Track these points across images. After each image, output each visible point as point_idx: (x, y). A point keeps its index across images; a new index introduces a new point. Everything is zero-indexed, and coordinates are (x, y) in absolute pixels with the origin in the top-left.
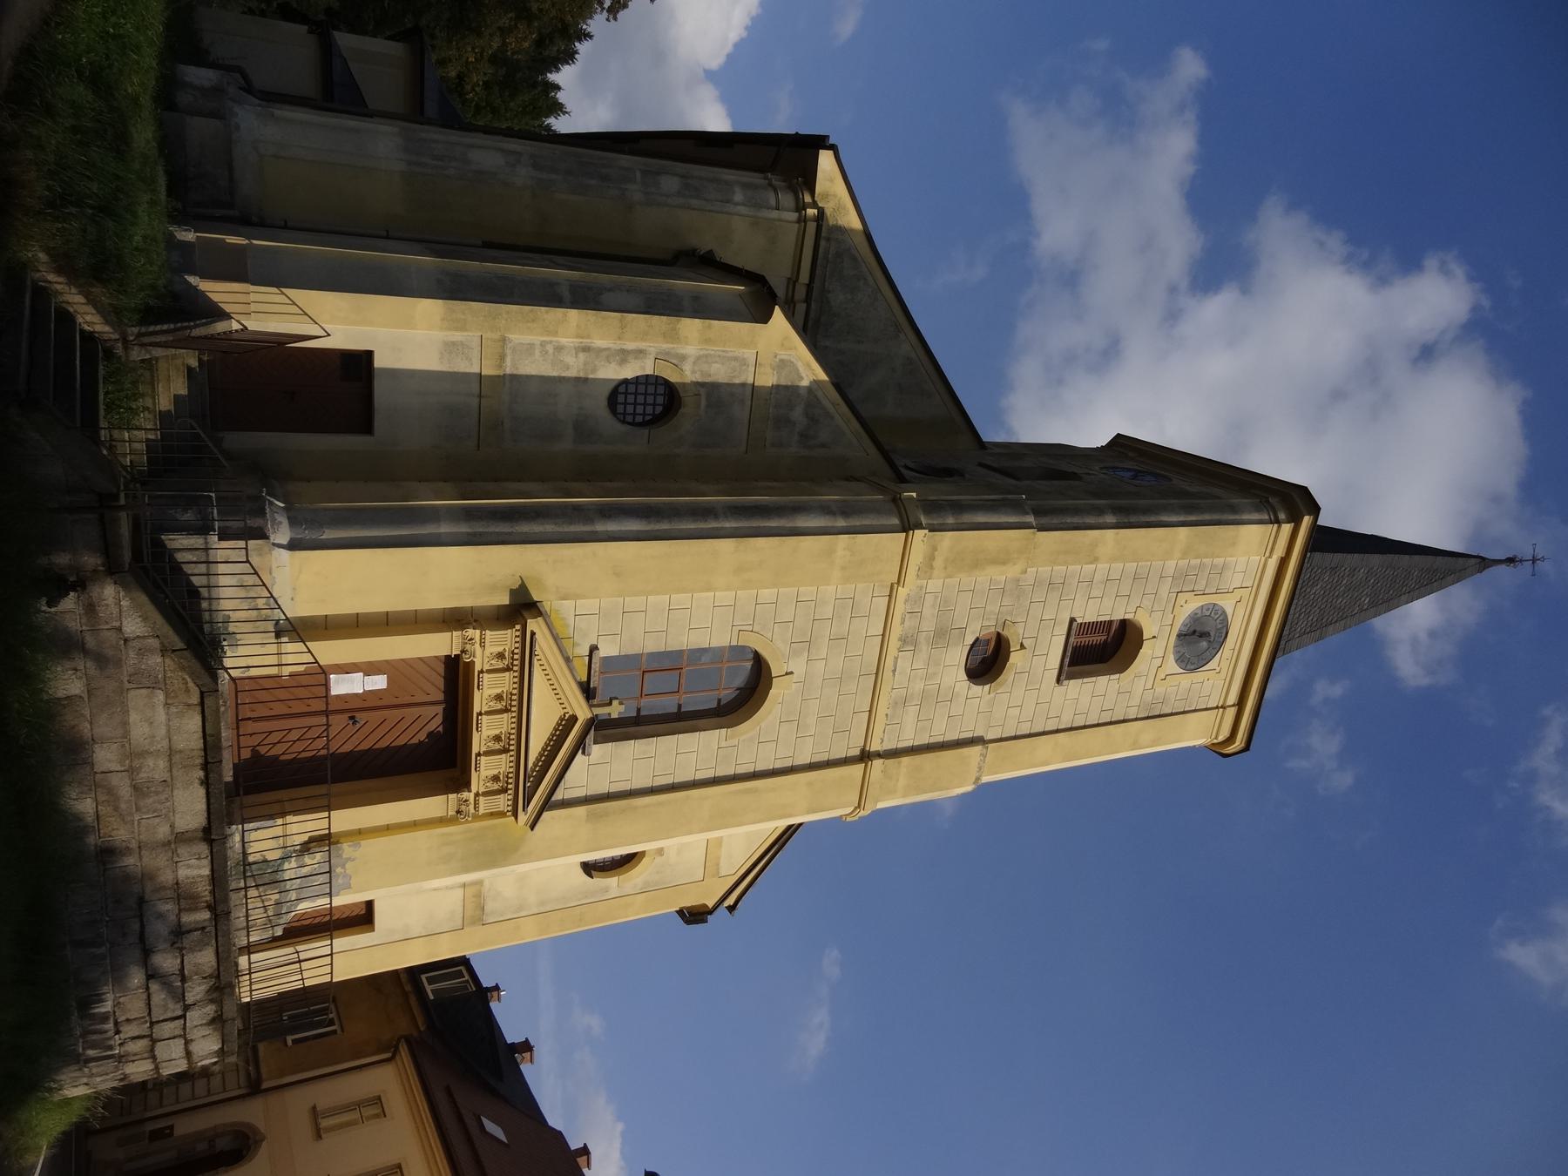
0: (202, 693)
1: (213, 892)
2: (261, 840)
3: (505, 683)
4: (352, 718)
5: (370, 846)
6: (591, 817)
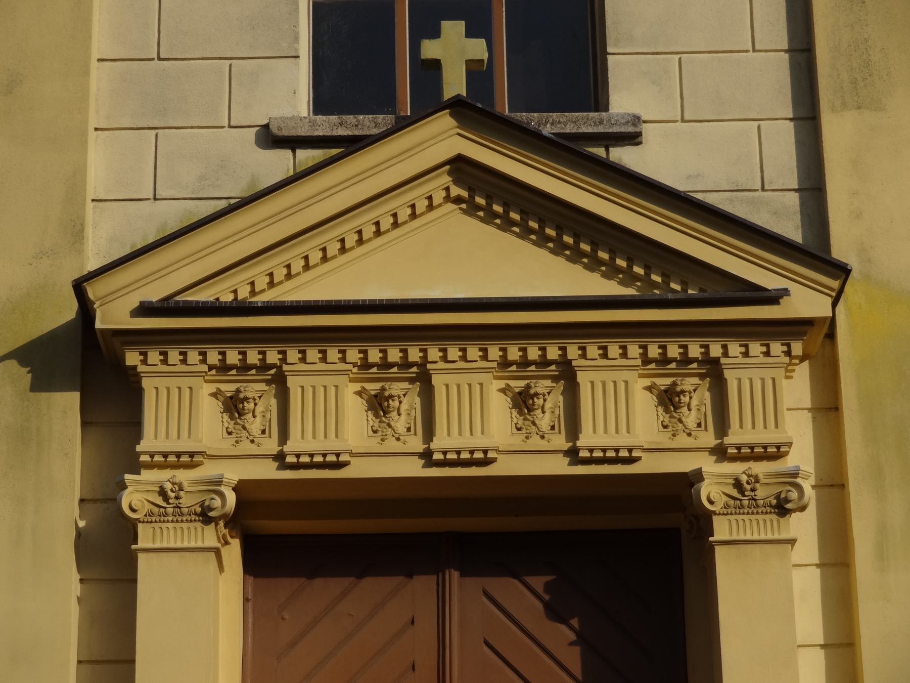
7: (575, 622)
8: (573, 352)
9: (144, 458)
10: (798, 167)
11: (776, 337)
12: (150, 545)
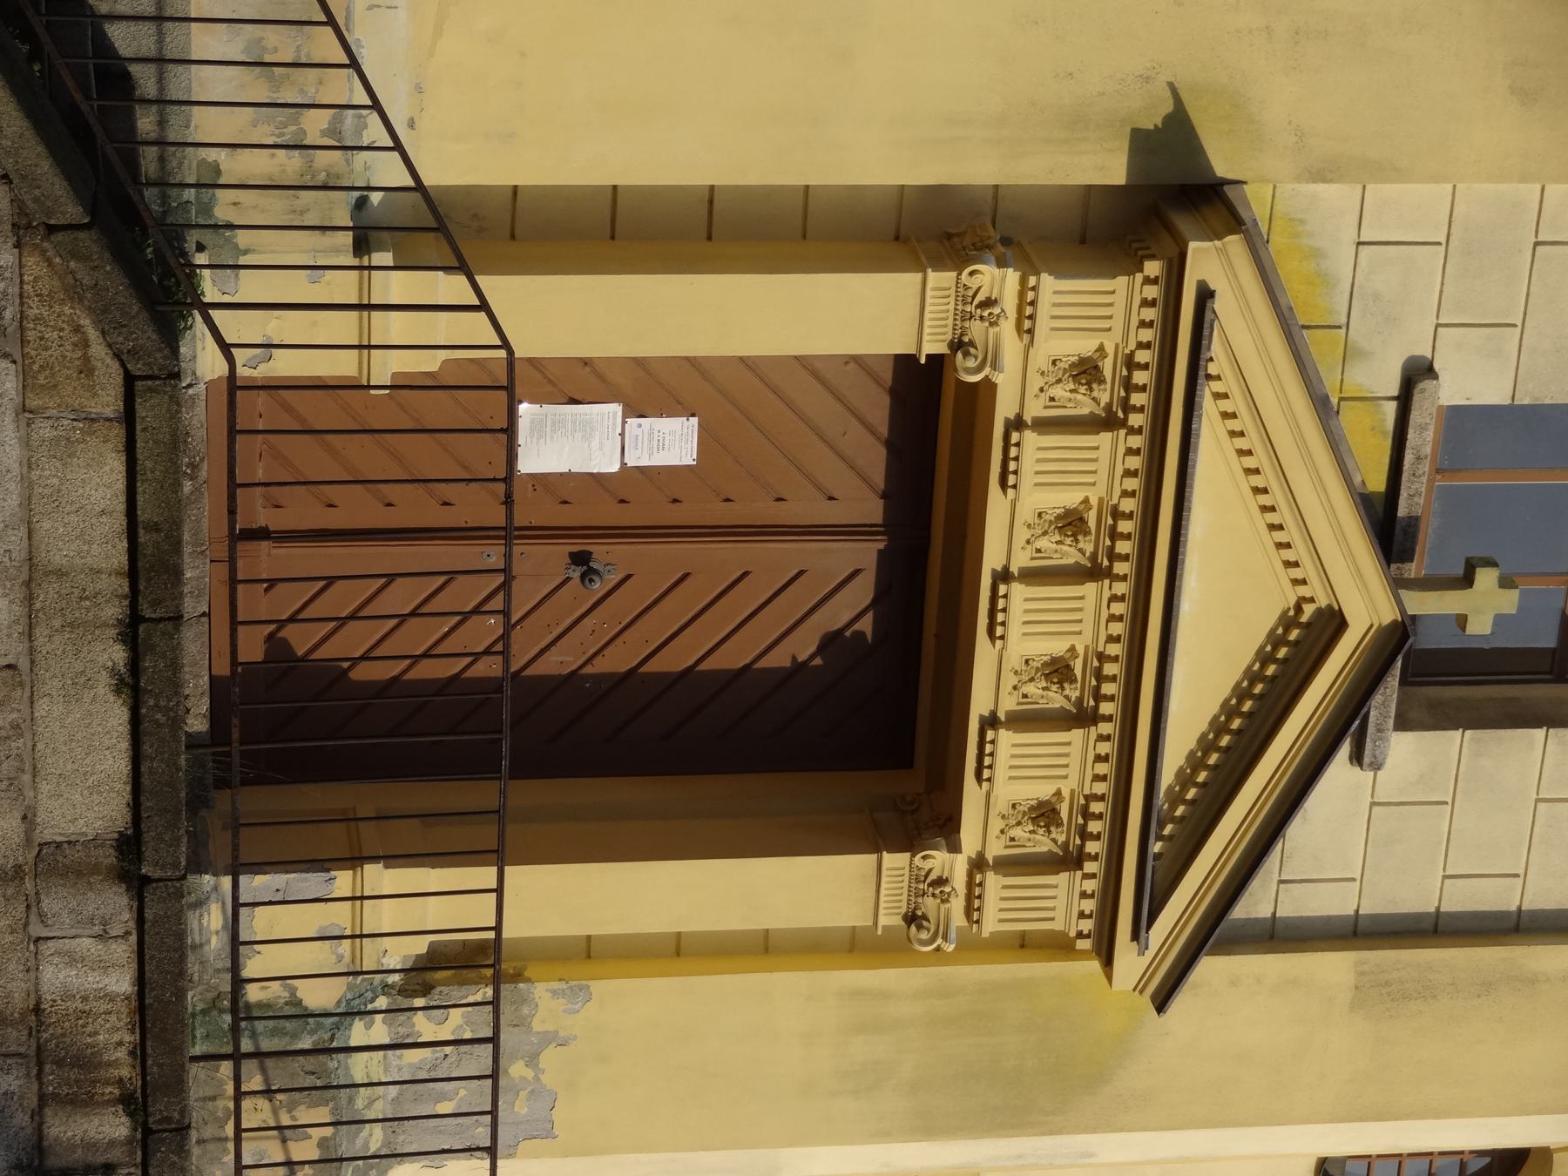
0: (130, 380)
1: (140, 1054)
2: (297, 931)
3: (1095, 472)
4: (580, 559)
5: (624, 1000)
6: (1364, 994)
7: (818, 661)
8: (1105, 728)
9: (1032, 281)
10: (1301, 918)
11: (1099, 925)
12: (930, 285)
